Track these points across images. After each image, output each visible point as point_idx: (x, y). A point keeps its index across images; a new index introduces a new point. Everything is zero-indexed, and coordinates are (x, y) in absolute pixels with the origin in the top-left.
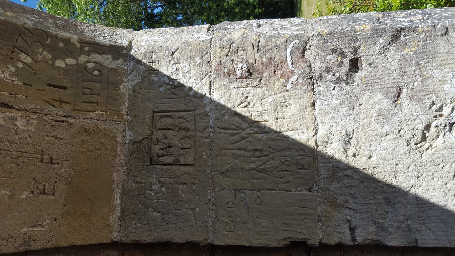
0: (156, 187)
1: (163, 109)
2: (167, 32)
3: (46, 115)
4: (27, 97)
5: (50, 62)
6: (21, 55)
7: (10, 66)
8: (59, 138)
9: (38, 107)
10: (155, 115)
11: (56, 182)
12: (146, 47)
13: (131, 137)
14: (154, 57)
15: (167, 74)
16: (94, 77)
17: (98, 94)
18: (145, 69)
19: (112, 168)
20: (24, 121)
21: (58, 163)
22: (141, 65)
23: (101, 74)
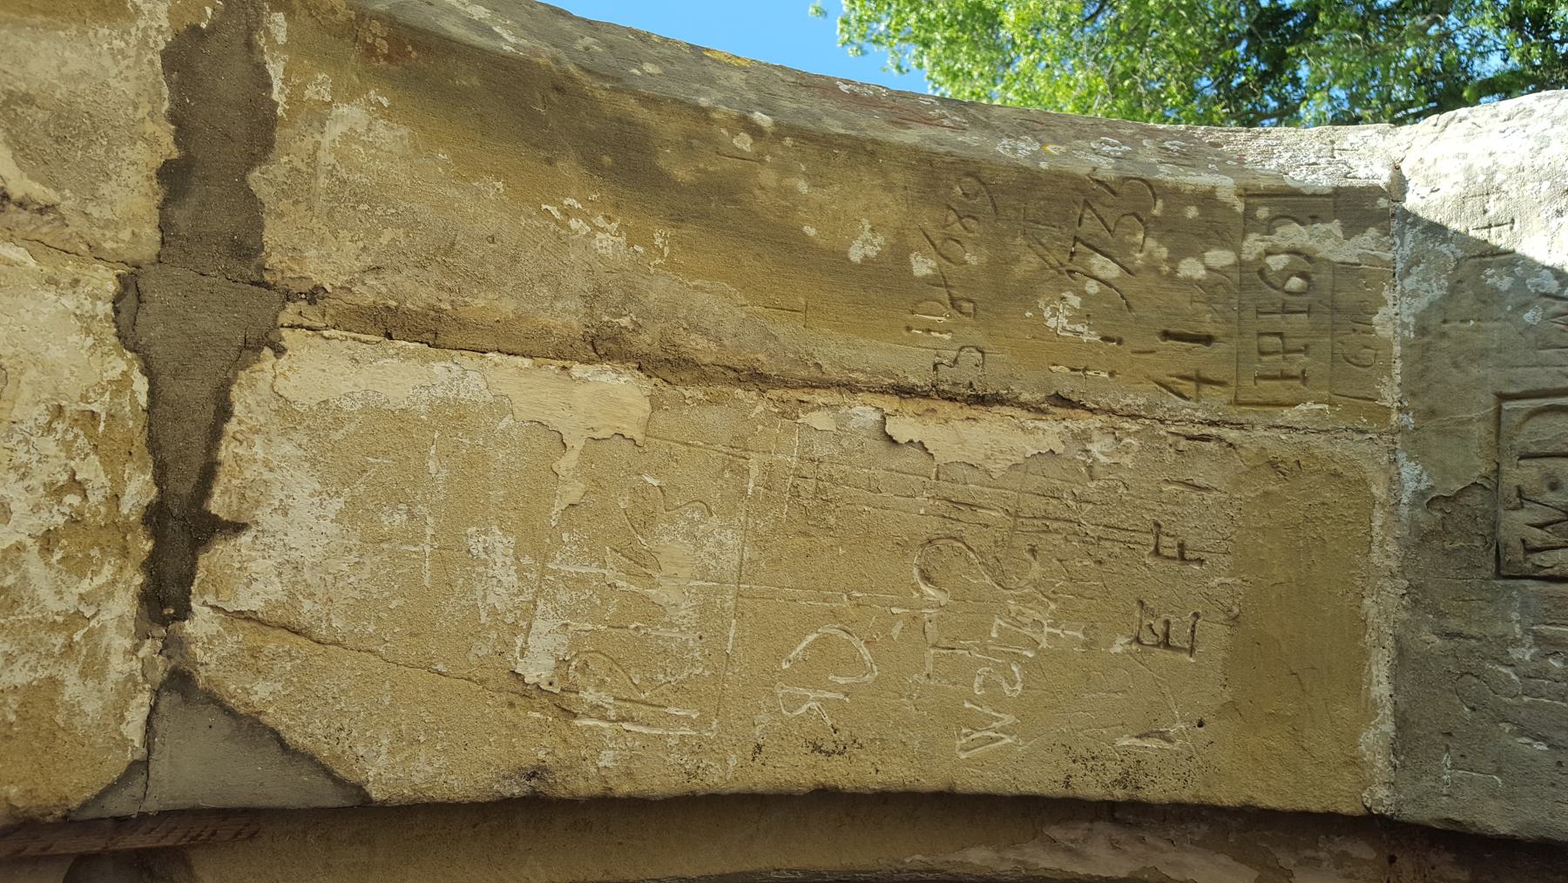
0: (1525, 654)
1: (1540, 387)
2: (1532, 111)
3: (1162, 422)
4: (1111, 374)
5: (1166, 268)
6: (1093, 261)
7: (1069, 295)
8: (1200, 488)
9: (1141, 401)
10: (1507, 406)
11: (1196, 615)
12: (1461, 178)
13: (1419, 482)
14: (1494, 207)
15: (1549, 263)
16: (1288, 298)
17: (1305, 350)
18: (1460, 254)
19: (1358, 583)
20: (1109, 440)
21: (1201, 561)
22: (1444, 241)
23: (1310, 286)
